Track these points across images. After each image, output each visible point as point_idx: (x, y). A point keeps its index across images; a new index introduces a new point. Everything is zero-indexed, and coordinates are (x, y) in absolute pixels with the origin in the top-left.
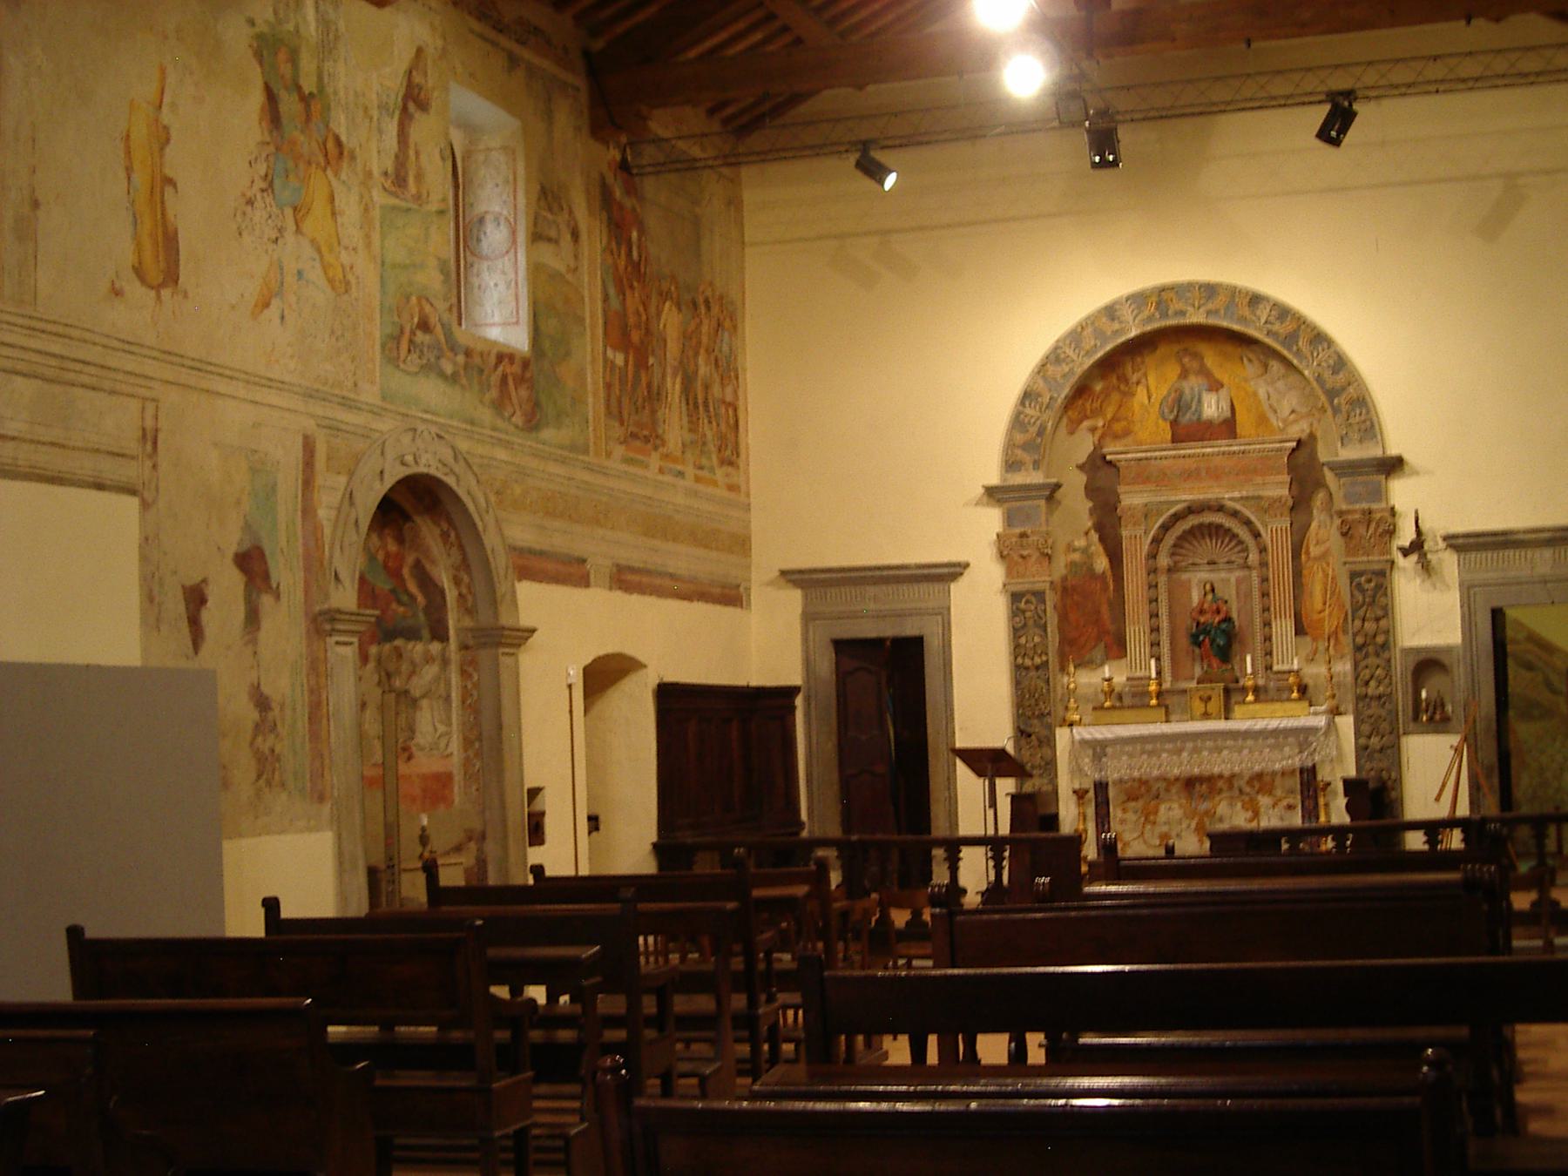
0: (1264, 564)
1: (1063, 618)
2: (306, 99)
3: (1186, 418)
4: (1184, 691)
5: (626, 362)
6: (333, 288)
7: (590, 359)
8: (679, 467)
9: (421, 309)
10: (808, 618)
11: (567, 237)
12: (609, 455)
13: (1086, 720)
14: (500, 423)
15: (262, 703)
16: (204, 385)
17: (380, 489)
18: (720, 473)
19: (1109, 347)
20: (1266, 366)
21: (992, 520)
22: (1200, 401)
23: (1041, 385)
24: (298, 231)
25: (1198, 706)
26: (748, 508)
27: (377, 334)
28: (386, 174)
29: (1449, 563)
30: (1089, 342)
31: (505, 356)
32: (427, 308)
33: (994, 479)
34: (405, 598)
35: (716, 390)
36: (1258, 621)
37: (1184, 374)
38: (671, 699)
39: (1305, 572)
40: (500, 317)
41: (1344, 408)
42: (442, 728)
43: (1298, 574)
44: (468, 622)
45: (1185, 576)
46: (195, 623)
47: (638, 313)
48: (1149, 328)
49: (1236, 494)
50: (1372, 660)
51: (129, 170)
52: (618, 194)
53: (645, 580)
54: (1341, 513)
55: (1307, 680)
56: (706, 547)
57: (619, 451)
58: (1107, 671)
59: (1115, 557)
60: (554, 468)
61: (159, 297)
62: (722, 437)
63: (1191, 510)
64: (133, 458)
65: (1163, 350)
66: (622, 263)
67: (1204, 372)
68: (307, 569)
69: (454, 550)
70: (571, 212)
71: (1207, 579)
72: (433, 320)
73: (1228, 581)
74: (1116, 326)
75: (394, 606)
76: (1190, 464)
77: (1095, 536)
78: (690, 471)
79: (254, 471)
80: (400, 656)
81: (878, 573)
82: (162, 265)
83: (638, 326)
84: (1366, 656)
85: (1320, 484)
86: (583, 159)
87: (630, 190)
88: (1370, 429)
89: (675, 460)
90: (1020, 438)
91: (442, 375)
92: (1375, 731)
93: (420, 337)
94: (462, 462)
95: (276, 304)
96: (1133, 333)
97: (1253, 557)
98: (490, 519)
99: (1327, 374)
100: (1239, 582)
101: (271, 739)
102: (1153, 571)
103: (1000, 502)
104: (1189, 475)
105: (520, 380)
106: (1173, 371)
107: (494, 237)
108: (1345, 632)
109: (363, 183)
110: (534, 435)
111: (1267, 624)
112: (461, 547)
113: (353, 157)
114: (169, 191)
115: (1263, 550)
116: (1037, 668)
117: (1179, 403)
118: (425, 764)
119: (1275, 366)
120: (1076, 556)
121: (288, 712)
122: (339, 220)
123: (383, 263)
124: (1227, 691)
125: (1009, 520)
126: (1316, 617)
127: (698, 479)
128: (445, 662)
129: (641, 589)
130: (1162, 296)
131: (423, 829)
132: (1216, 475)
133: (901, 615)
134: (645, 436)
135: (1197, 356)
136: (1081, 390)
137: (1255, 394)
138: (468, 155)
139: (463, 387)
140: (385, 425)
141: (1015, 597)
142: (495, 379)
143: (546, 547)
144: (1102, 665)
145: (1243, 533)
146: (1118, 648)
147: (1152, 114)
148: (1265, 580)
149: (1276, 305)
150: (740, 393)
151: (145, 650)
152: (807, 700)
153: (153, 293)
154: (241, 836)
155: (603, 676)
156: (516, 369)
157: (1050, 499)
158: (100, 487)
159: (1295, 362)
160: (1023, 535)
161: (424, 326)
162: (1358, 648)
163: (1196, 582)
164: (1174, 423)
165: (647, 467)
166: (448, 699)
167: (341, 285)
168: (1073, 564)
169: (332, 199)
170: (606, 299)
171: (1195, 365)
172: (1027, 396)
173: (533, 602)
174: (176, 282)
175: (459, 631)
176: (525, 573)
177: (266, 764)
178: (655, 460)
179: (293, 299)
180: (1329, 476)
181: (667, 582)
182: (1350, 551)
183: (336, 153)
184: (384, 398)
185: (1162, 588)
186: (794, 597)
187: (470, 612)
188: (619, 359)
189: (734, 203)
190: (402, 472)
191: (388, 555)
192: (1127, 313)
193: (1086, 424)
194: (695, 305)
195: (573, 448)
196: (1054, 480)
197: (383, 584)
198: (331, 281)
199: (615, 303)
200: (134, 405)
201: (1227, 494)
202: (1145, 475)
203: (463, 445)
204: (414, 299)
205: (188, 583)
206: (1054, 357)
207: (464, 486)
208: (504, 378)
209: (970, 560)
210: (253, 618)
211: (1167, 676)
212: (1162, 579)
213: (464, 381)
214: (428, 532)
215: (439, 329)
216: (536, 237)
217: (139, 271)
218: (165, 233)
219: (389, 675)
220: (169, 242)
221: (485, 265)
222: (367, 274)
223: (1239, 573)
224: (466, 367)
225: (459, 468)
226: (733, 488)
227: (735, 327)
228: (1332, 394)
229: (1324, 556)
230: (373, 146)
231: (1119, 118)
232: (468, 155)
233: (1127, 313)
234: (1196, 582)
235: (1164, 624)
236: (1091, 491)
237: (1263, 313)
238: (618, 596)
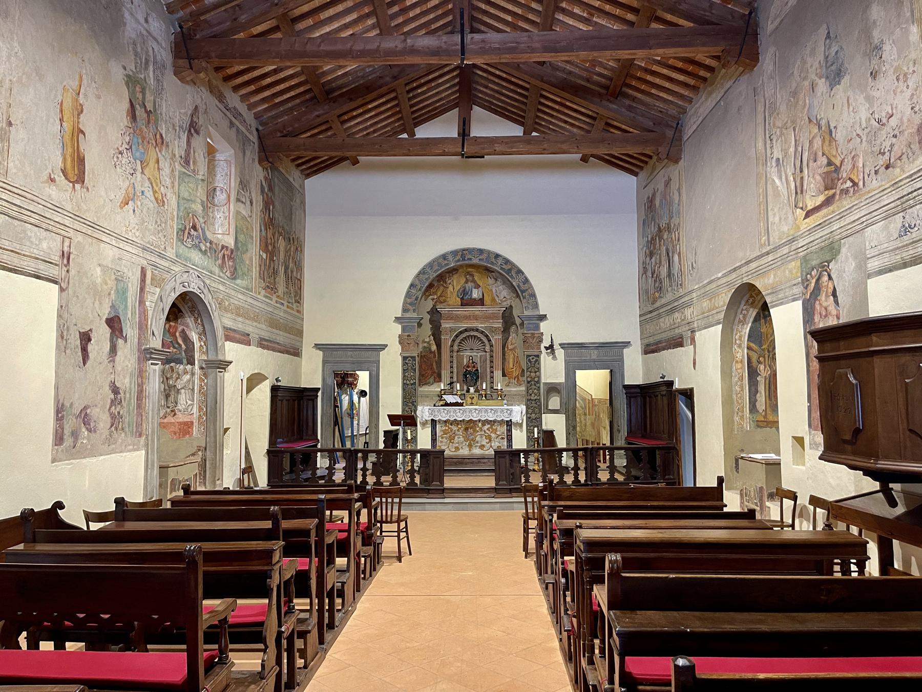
0: (492, 351)
1: (420, 367)
2: (149, 113)
7: (254, 254)
14: (221, 274)
15: (115, 390)
21: (398, 329)
23: (417, 282)
24: (142, 173)
29: (560, 353)
33: (400, 315)
37: (467, 282)
38: (275, 389)
40: (222, 230)
42: (189, 402)
46: (84, 350)
50: (534, 387)
51: (61, 120)
57: (263, 292)
59: (439, 346)
60: (240, 296)
63: (466, 330)
64: (56, 265)
68: (140, 328)
71: (471, 354)
72: (198, 226)
78: (286, 304)
80: (173, 371)
86: (258, 173)
88: (536, 306)
90: (409, 301)
91: (201, 250)
92: (533, 412)
93: (192, 232)
97: (488, 348)
98: (216, 314)
99: (521, 285)
102: (452, 351)
103: (401, 323)
104: (467, 318)
105: (230, 258)
106: (463, 280)
109: (172, 159)
112: (203, 325)
113: (167, 146)
114: (81, 136)
115: (491, 346)
117: (464, 292)
118: (181, 418)
120: (425, 345)
121: (128, 395)
125: (404, 330)
127: (288, 307)
128: (193, 374)
132: (476, 318)
135: (472, 276)
136: (431, 286)
141: (404, 358)
142: (221, 255)
148: (492, 356)
149: (504, 258)
151: (403, 410)
152: (323, 393)
155: (253, 381)
156: (228, 253)
158: (38, 277)
160: (409, 336)
161: (194, 228)
164: (462, 299)
166: (193, 390)
167: (160, 201)
169: (158, 162)
174: (83, 182)
175: (199, 361)
176: (228, 338)
177: (115, 419)
179: (139, 203)
181: (276, 346)
183: (160, 142)
192: (450, 257)
195: (247, 289)
198: (156, 199)
199: (264, 233)
200: (59, 238)
202: (451, 317)
203: (208, 282)
207: (207, 298)
208: (224, 255)
210: (113, 350)
212: (455, 354)
217: (64, 172)
218: (78, 155)
219: (167, 379)
220: (81, 161)
225: (206, 291)
226: (298, 311)
230: (176, 142)
233: (450, 257)
235: (455, 370)
237: (500, 261)
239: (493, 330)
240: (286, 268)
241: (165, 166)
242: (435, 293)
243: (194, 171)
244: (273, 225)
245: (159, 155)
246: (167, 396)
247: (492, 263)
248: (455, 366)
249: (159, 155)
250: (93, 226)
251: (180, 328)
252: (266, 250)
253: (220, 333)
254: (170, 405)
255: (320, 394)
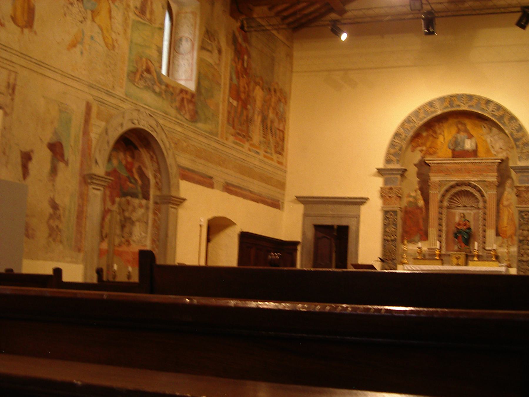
0: (485, 207)
3: (459, 149)
4: (449, 255)
5: (238, 105)
6: (107, 47)
7: (222, 100)
8: (258, 151)
9: (147, 63)
10: (306, 215)
11: (216, 52)
12: (227, 139)
13: (410, 263)
14: (179, 116)
15: (55, 206)
16: (40, 71)
17: (121, 131)
18: (275, 156)
19: (475, 111)
20: (490, 129)
21: (379, 182)
22: (464, 143)
24: (93, 20)
25: (455, 261)
26: (285, 172)
27: (126, 69)
28: (136, 8)
30: (421, 115)
31: (183, 91)
32: (150, 64)
33: (381, 166)
34: (133, 181)
35: (276, 124)
36: (481, 230)
37: (459, 131)
39: (501, 211)
40: (186, 77)
41: (521, 146)
42: (143, 234)
43: (498, 211)
44: (158, 193)
45: (453, 211)
47: (244, 87)
48: (445, 111)
49: (476, 180)
52: (240, 40)
53: (238, 190)
54: (517, 187)
55: (499, 255)
56: (266, 183)
57: (232, 138)
58: (420, 245)
59: (427, 201)
61: (22, 32)
62: (277, 143)
63: (458, 184)
65: (451, 121)
66: (239, 67)
67: (467, 131)
69: (155, 165)
70: (219, 43)
73: (470, 214)
74: (433, 109)
75: (128, 183)
76: (459, 166)
77: (419, 192)
78: (262, 152)
79: (60, 111)
81: (333, 200)
82: (26, 18)
83: (244, 93)
84: (523, 245)
85: (509, 177)
86: (225, 25)
87: (246, 39)
89: (256, 148)
90: (392, 151)
91: (154, 92)
93: (145, 74)
94: (160, 127)
95: (79, 47)
96: (439, 112)
97: (481, 205)
99: (515, 133)
100: (475, 214)
101: (57, 222)
102: (441, 207)
103: (382, 175)
104: (458, 171)
105: (190, 101)
106: (454, 130)
107: (185, 46)
108: (515, 235)
109: (126, 9)
110: (194, 124)
111: (484, 231)
112: (158, 163)
115: (485, 202)
116: (392, 240)
117: (456, 143)
119: (495, 130)
120: (411, 199)
121: (67, 212)
122: (113, 20)
123: (131, 42)
124: (467, 256)
125: (386, 182)
126: (504, 229)
128: (147, 208)
129: (236, 194)
130: (451, 98)
131: (129, 272)
132: (468, 171)
133: (341, 217)
134: (243, 134)
135: (464, 124)
136: (417, 135)
137: (486, 141)
138: (178, 14)
139: (164, 99)
140: (126, 106)
141: (386, 212)
142: (179, 98)
143: (196, 170)
144: (417, 243)
145: (477, 195)
146: (425, 236)
147: (450, 13)
148: (485, 214)
150: (286, 127)
152: (302, 248)
153: (19, 29)
154: (38, 259)
156: (189, 97)
157: (402, 175)
159: (502, 127)
161: (148, 71)
162: (520, 241)
163: (458, 214)
164: (453, 151)
165: (243, 147)
166: (147, 223)
167: (111, 46)
168: (410, 202)
169: (110, 11)
170: (231, 79)
171: (463, 128)
172: (397, 135)
173: (186, 189)
176: (185, 177)
177: (54, 233)
178: (247, 145)
180: (513, 173)
182: (519, 202)
184: (126, 95)
185: (444, 217)
186: (300, 208)
187: (159, 189)
188: (235, 103)
189: (290, 56)
190: (131, 126)
191: (127, 162)
192: (437, 105)
193: (419, 148)
194: (270, 90)
196: (404, 168)
197: (124, 173)
198: (106, 43)
199: (235, 81)
201: (472, 179)
202: (441, 170)
203: (161, 121)
204: (144, 59)
205: (24, 150)
206: (408, 120)
207: (159, 136)
208: (182, 100)
209: (369, 197)
210: (54, 171)
211: (444, 249)
213: (164, 96)
214: (145, 155)
215: (155, 74)
216: (202, 48)
221: (180, 56)
222: (123, 45)
223: (475, 211)
224: (166, 91)
227: (286, 102)
228: (516, 140)
229: (509, 206)
231: (436, 15)
232: (178, 14)
233: (437, 105)
234: (458, 214)
235: (444, 228)
236: (419, 175)
237: (491, 107)
238: (226, 194)
239: (487, 185)
240: (264, 120)
241: (118, 16)
242: (423, 144)
243: (150, 20)
244: (247, 74)
245: (112, 5)
246: (123, 227)
247: (483, 109)
248: (444, 224)
249: (112, 5)
250: (40, 64)
251: (136, 165)
252: (237, 97)
253: (174, 171)
254: (126, 235)
255: (299, 248)
